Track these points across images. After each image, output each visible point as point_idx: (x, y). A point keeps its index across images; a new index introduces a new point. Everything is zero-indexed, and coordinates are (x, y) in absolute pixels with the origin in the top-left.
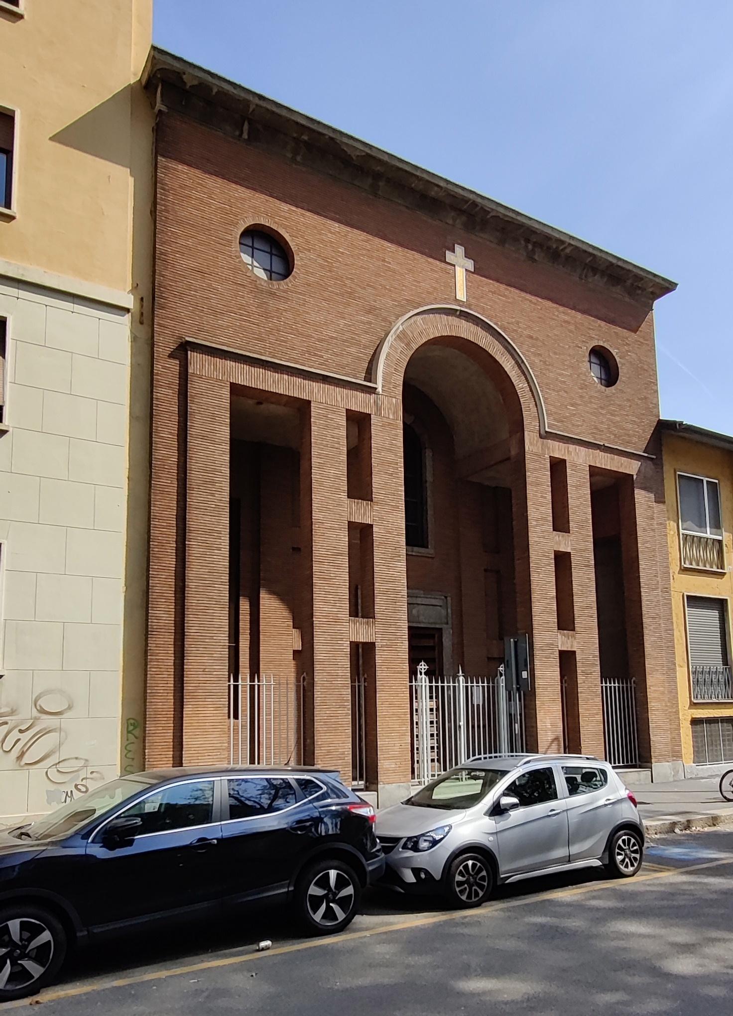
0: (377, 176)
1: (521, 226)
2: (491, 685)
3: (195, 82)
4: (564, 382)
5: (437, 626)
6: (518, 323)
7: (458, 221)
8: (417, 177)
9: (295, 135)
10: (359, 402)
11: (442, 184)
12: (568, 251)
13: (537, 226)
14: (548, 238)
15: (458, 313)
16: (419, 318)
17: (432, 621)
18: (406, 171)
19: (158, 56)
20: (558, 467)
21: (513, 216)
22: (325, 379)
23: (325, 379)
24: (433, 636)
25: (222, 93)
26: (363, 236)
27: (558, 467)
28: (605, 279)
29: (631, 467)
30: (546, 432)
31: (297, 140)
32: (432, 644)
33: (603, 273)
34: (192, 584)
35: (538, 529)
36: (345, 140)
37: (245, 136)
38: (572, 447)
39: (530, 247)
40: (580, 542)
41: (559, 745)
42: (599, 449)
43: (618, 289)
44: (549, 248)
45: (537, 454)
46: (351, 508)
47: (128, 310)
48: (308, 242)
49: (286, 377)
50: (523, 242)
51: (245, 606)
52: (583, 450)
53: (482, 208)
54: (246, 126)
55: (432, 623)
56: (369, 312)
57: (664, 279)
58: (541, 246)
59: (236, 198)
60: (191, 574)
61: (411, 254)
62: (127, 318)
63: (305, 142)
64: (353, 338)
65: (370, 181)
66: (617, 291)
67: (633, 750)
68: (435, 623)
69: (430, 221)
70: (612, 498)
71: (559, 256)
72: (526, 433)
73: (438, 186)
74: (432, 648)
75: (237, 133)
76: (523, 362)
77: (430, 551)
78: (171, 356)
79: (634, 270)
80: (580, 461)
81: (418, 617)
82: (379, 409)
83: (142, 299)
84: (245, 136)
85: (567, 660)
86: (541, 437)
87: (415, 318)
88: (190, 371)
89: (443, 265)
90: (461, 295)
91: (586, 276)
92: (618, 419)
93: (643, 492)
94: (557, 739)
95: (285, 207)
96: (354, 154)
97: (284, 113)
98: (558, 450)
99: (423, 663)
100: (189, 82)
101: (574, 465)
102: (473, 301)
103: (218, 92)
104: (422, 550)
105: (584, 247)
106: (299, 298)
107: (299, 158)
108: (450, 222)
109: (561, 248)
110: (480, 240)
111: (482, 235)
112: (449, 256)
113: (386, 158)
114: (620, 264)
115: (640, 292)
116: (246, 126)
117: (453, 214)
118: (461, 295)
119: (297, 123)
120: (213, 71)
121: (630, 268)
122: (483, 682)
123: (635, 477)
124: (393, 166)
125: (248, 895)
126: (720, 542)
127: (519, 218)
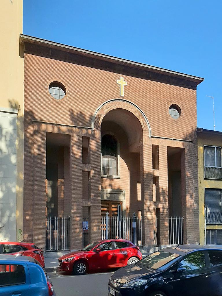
2: (176, 219)
3: (34, 41)
19: (21, 36)
20: (155, 148)
26: (139, 79)
27: (155, 148)
37: (50, 54)
45: (148, 143)
51: (139, 198)
63: (69, 52)
70: (176, 157)
72: (144, 138)
80: (163, 146)
84: (50, 54)
90: (122, 94)
98: (156, 142)
102: (126, 95)
116: (50, 51)
118: (122, 94)
122: (171, 218)
126: (221, 168)
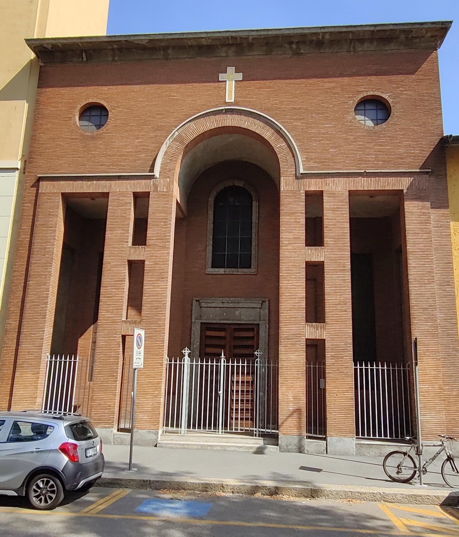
0: (165, 49)
1: (277, 36)
4: (327, 133)
5: (255, 322)
6: (282, 102)
7: (230, 52)
8: (186, 38)
9: (110, 48)
10: (141, 186)
11: (203, 36)
12: (327, 36)
13: (287, 32)
14: (303, 35)
15: (224, 111)
16: (192, 123)
17: (251, 318)
18: (178, 39)
20: (314, 200)
21: (265, 33)
22: (119, 178)
23: (119, 178)
24: (253, 329)
25: (64, 45)
28: (375, 43)
29: (404, 184)
30: (302, 174)
31: (113, 49)
32: (252, 336)
33: (371, 40)
34: (27, 305)
35: (290, 247)
36: (132, 38)
37: (85, 59)
38: (329, 180)
39: (294, 46)
40: (337, 255)
41: (300, 418)
42: (361, 176)
43: (392, 46)
44: (312, 42)
46: (130, 251)
47: (17, 169)
48: (118, 102)
49: (95, 182)
50: (287, 46)
52: (342, 180)
53: (241, 38)
54: (84, 54)
55: (251, 320)
56: (156, 130)
57: (433, 23)
58: (304, 42)
59: (76, 94)
60: (28, 299)
61: (190, 86)
62: (17, 173)
64: (143, 149)
65: (162, 52)
66: (392, 47)
67: (256, 427)
68: (255, 320)
69: (208, 60)
71: (323, 43)
73: (203, 38)
74: (253, 338)
75: (80, 60)
76: (281, 129)
77: (252, 270)
78: (32, 186)
79: (396, 28)
81: (240, 316)
82: (156, 187)
83: (25, 161)
85: (316, 350)
86: (297, 178)
87: (189, 124)
88: (40, 192)
89: (216, 84)
91: (354, 48)
92: (389, 147)
93: (416, 203)
94: (298, 410)
95: (105, 88)
96: (144, 42)
97: (95, 40)
99: (183, 351)
100: (49, 47)
101: (333, 195)
103: (62, 45)
104: (246, 270)
105: (337, 30)
106: (109, 136)
107: (116, 59)
108: (224, 55)
109: (320, 37)
110: (250, 57)
111: (251, 54)
112: (222, 77)
113: (161, 37)
114: (378, 28)
115: (418, 40)
116: (84, 54)
117: (224, 49)
119: (104, 42)
120: (54, 37)
121: (392, 27)
123: (405, 191)
124: (168, 39)
125: (141, 493)
127: (270, 33)
